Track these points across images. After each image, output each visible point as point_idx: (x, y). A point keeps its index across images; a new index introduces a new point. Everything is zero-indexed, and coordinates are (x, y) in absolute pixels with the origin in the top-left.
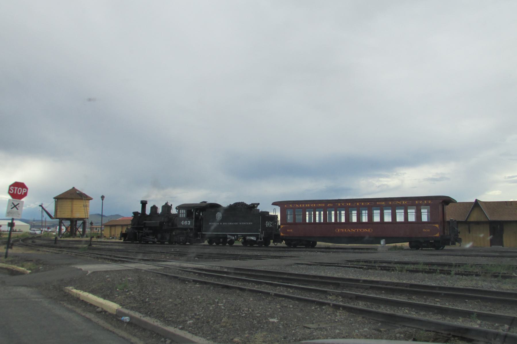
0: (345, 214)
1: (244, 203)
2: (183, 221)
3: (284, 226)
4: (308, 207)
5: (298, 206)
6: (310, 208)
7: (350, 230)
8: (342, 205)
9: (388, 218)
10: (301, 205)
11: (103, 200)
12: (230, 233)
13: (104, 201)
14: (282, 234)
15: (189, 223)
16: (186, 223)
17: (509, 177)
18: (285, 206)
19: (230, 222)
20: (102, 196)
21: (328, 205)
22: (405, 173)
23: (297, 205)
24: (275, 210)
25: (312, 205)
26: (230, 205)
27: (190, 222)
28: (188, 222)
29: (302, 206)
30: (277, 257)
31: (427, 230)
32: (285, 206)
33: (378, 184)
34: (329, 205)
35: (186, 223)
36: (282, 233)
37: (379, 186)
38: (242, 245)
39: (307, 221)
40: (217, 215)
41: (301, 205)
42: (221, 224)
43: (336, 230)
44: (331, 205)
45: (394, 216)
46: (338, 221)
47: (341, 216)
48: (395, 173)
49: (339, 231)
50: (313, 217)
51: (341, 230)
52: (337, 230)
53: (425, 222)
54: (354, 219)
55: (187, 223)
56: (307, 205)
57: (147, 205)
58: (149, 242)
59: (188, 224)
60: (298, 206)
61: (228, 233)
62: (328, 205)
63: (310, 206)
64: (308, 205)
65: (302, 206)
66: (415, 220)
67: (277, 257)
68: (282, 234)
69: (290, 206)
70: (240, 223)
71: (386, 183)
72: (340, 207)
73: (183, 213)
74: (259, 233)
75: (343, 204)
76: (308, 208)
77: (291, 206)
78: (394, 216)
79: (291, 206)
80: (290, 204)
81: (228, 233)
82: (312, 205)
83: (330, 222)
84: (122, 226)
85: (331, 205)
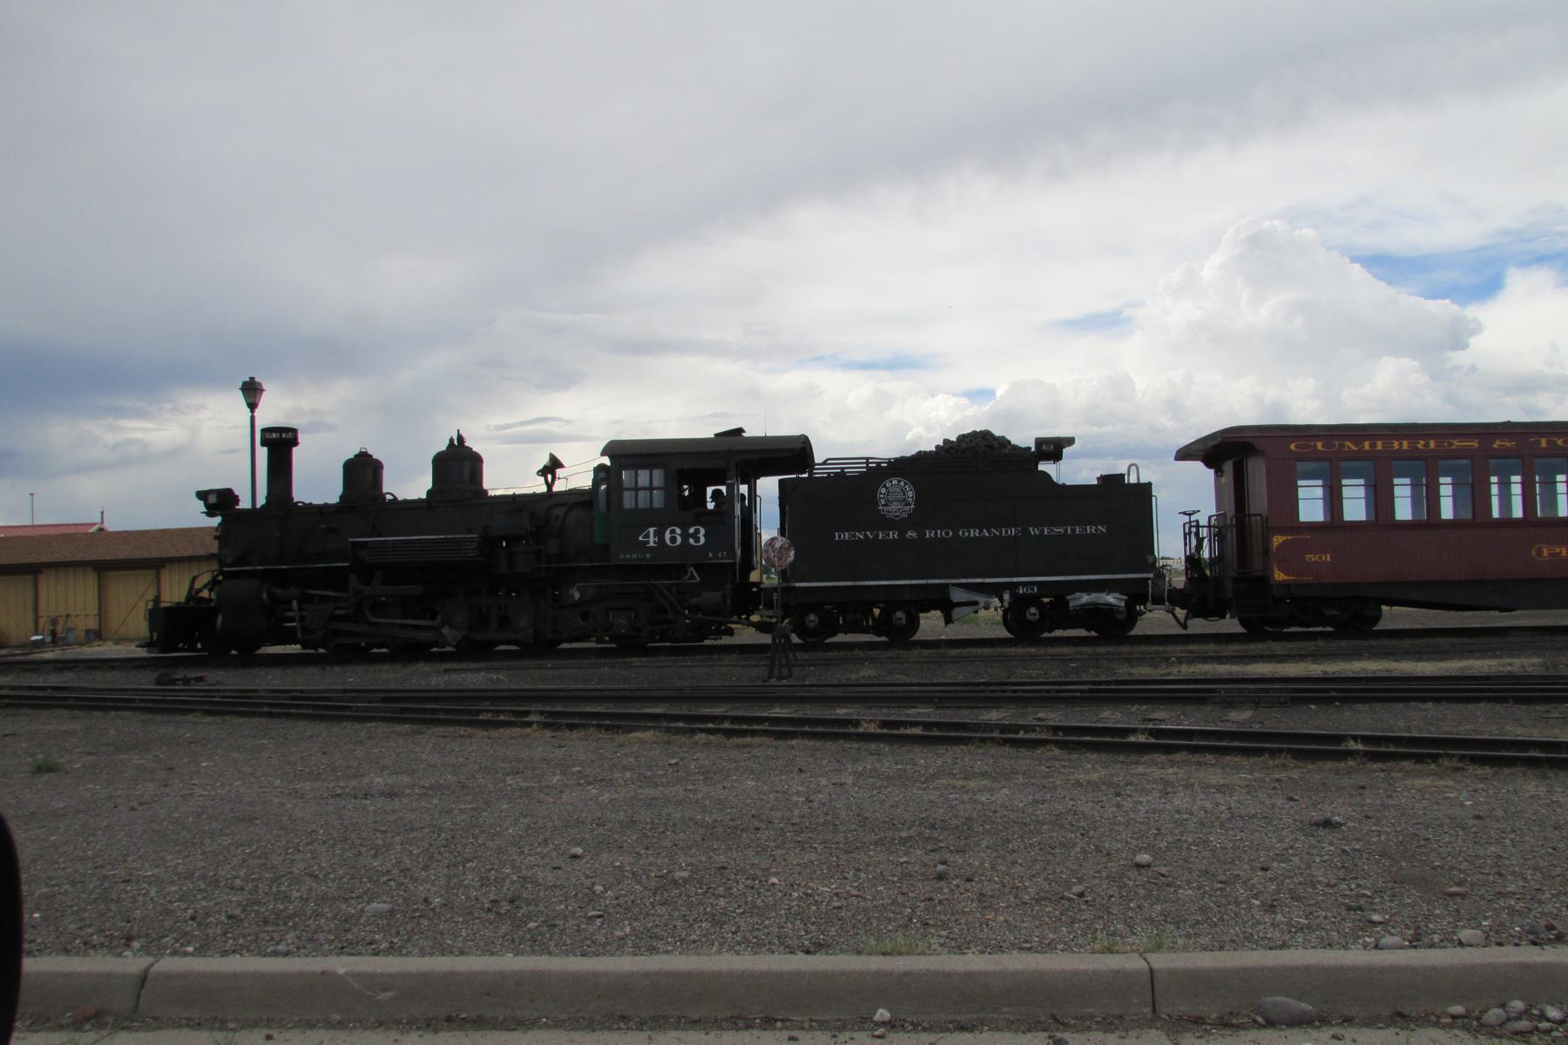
0: (1523, 483)
1: (994, 438)
2: (652, 530)
3: (1289, 538)
4: (1400, 450)
5: (1355, 448)
6: (1413, 456)
7: (866, 536)
8: (1555, 444)
9: (1355, 507)
10: (1367, 446)
11: (252, 406)
12: (964, 581)
13: (257, 412)
14: (1279, 576)
15: (695, 536)
16: (673, 540)
17: (499, 428)
18: (1292, 447)
19: (969, 526)
20: (245, 384)
21: (1495, 446)
22: (203, 407)
23: (1348, 443)
24: (1133, 468)
25: (1422, 442)
26: (946, 441)
27: (702, 531)
28: (692, 531)
29: (1373, 445)
30: (70, 665)
31: (1321, 558)
32: (1292, 447)
33: (111, 438)
34: (1498, 442)
35: (673, 540)
36: (1279, 569)
37: (115, 447)
38: (1009, 635)
39: (1496, 514)
40: (883, 490)
41: (1367, 446)
42: (911, 534)
43: (1533, 553)
44: (1507, 444)
45: (1334, 500)
46: (1539, 515)
47: (1340, 498)
48: (170, 406)
49: (1550, 555)
50: (1538, 492)
51: (1558, 550)
52: (1539, 552)
53: (1404, 525)
54: (1403, 510)
55: (685, 536)
56: (1396, 445)
57: (295, 450)
58: (564, 646)
59: (692, 541)
60: (1355, 448)
61: (953, 581)
62: (1495, 446)
63: (1413, 449)
64: (1401, 445)
65: (1373, 445)
66: (1325, 516)
67: (70, 665)
68: (1279, 576)
69: (1315, 446)
70: (1033, 531)
71: (139, 435)
72: (1544, 455)
73: (651, 488)
74: (1151, 575)
75: (1560, 442)
76: (1401, 456)
77: (1319, 445)
78: (1334, 500)
79: (1319, 445)
80: (1317, 437)
81: (953, 581)
82: (1422, 442)
83: (1548, 514)
84: (155, 565)
85: (1507, 444)
